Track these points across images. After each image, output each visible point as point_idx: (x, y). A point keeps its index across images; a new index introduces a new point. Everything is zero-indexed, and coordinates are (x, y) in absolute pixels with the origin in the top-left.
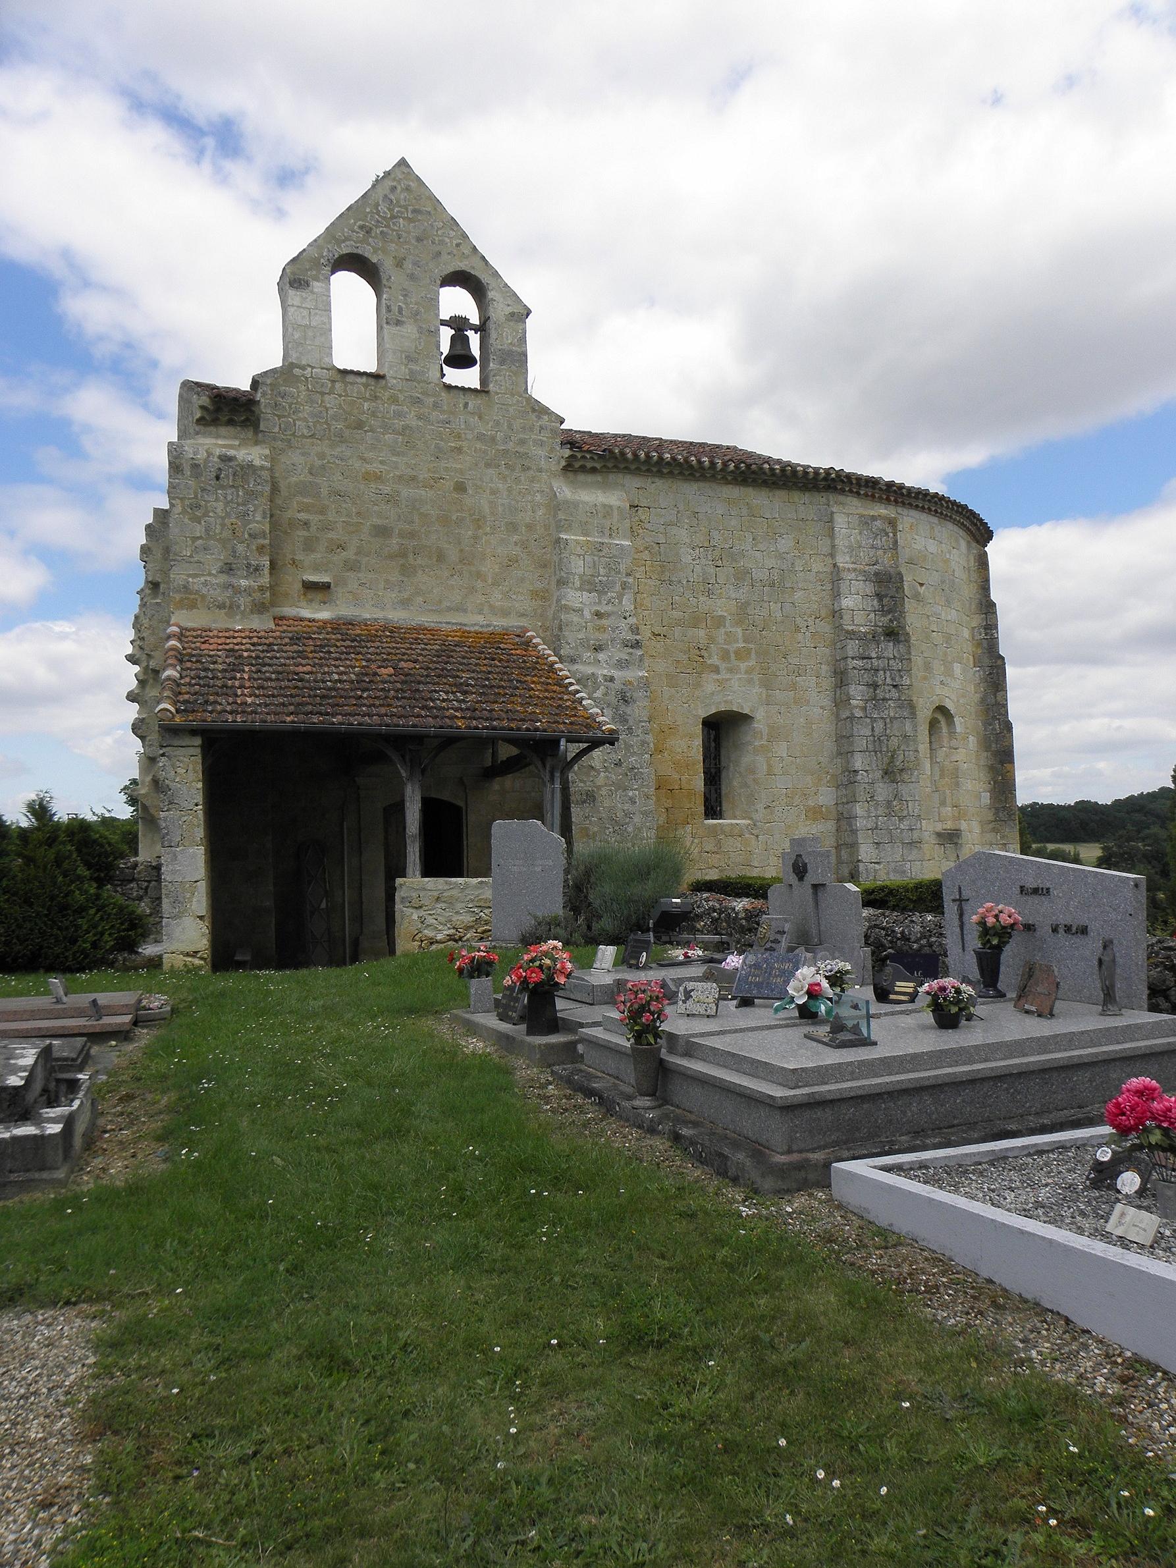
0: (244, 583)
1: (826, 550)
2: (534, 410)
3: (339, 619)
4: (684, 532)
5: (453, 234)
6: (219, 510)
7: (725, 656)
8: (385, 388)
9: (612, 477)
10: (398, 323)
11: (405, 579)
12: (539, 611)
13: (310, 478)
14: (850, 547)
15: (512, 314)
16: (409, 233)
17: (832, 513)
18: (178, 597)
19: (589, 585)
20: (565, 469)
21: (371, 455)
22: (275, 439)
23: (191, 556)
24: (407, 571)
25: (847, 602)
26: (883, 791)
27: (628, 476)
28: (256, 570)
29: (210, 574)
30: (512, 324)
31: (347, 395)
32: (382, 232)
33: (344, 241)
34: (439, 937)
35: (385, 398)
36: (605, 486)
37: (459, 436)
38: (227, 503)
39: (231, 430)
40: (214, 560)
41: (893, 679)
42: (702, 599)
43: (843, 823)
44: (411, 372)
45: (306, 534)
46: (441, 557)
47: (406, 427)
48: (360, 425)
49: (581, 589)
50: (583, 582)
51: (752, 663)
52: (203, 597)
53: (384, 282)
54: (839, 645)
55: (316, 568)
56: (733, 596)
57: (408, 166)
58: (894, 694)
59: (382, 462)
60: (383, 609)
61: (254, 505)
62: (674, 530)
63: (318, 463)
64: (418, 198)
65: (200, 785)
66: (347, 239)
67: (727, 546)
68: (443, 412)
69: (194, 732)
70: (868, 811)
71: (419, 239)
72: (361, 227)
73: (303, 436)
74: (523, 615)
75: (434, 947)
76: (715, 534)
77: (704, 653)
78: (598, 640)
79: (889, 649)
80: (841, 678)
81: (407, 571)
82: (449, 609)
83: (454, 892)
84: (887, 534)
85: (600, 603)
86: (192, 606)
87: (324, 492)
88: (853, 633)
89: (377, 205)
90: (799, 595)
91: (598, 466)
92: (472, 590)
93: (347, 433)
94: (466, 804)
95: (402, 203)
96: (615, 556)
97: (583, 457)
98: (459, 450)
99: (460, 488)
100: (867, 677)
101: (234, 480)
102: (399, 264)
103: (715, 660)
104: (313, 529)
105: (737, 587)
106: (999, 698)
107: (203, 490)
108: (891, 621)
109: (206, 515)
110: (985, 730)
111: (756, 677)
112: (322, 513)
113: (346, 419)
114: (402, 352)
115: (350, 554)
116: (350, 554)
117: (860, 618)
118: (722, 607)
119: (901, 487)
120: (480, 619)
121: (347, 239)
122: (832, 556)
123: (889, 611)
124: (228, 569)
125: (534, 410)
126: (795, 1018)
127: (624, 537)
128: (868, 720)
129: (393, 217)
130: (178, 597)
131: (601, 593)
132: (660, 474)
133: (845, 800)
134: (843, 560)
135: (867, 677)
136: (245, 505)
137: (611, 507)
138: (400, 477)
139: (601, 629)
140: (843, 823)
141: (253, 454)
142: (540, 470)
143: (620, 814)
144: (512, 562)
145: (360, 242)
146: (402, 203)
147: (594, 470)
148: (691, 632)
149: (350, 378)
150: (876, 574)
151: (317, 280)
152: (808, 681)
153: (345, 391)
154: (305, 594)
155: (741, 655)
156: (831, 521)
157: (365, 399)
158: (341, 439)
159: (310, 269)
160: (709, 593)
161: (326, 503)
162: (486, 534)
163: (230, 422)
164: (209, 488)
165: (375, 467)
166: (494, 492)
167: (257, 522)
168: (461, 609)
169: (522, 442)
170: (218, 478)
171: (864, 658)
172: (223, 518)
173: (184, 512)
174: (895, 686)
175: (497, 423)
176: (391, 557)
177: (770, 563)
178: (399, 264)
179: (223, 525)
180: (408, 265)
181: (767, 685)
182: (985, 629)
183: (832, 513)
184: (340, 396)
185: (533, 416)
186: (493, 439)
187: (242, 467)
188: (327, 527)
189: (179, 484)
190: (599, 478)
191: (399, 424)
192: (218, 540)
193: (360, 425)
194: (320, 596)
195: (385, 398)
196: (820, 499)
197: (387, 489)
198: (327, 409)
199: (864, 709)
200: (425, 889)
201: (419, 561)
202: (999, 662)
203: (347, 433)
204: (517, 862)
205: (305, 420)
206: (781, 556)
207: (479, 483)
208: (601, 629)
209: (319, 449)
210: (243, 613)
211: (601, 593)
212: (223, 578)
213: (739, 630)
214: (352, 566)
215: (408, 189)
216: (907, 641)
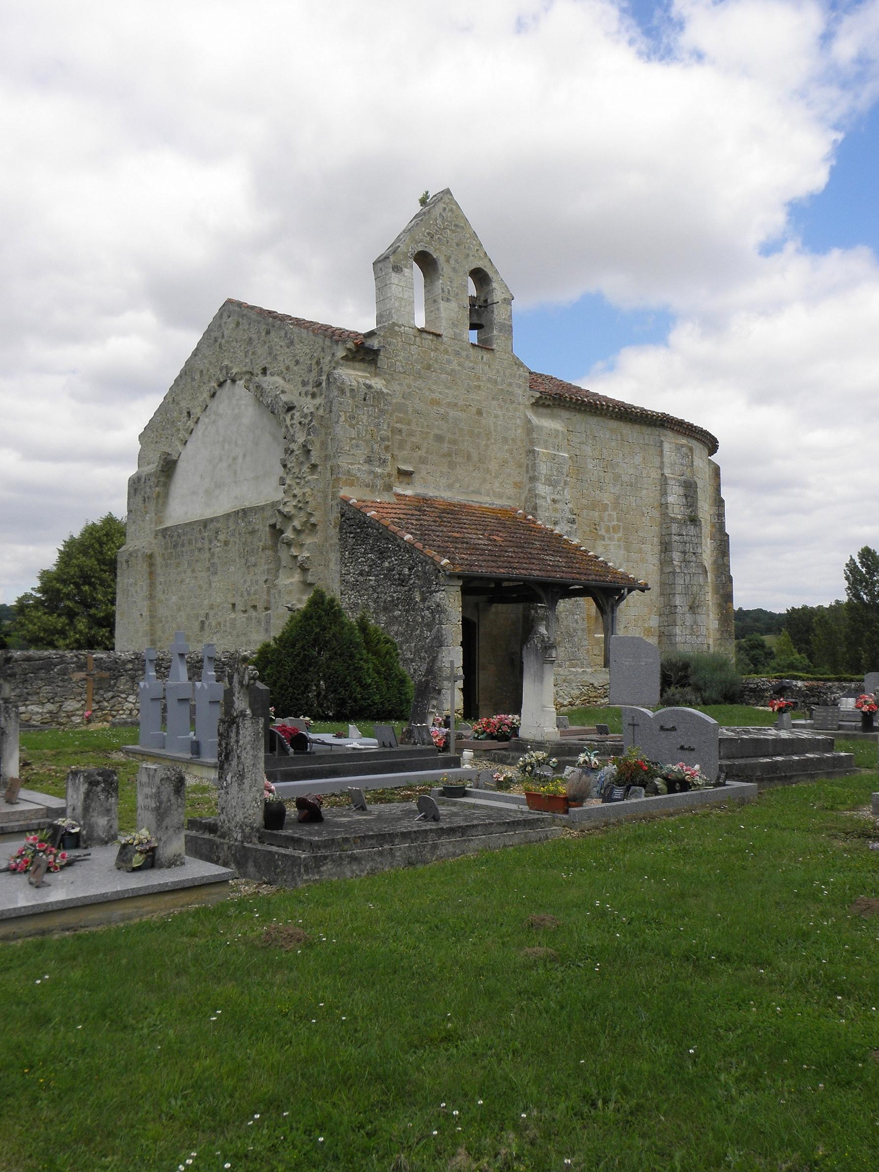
0: (379, 470)
1: (658, 464)
2: (516, 364)
3: (418, 495)
4: (589, 449)
5: (475, 242)
6: (364, 421)
7: (608, 531)
8: (442, 343)
9: (555, 410)
10: (448, 300)
11: (451, 471)
12: (518, 496)
13: (403, 401)
14: (671, 464)
15: (505, 299)
16: (452, 239)
17: (662, 441)
18: (344, 477)
19: (550, 482)
20: (533, 404)
21: (434, 387)
22: (385, 373)
23: (349, 451)
24: (452, 466)
25: (671, 499)
26: (689, 618)
27: (563, 411)
28: (384, 462)
29: (359, 463)
30: (505, 305)
31: (422, 347)
32: (439, 238)
33: (419, 242)
34: (565, 703)
35: (442, 350)
36: (553, 417)
37: (479, 379)
38: (369, 416)
39: (362, 365)
40: (361, 453)
41: (693, 549)
42: (598, 492)
43: (665, 639)
44: (455, 334)
45: (400, 437)
46: (469, 458)
47: (453, 370)
48: (429, 367)
49: (544, 484)
50: (546, 479)
51: (620, 535)
52: (358, 478)
53: (440, 272)
54: (664, 526)
55: (405, 462)
56: (612, 491)
57: (451, 195)
58: (694, 559)
59: (440, 393)
60: (439, 490)
61: (383, 419)
62: (584, 447)
63: (407, 391)
64: (457, 217)
65: (460, 609)
66: (421, 241)
67: (610, 459)
68: (471, 361)
69: (459, 577)
70: (682, 632)
71: (458, 245)
72: (429, 234)
73: (400, 372)
74: (509, 498)
75: (562, 708)
76: (604, 451)
77: (597, 527)
78: (556, 518)
79: (692, 530)
80: (666, 547)
81: (452, 466)
82: (473, 492)
83: (572, 677)
84: (688, 457)
85: (553, 493)
86: (352, 485)
87: (410, 410)
88: (674, 519)
89: (436, 219)
90: (644, 492)
91: (551, 403)
92: (485, 480)
93: (423, 372)
94: (479, 621)
95: (449, 219)
96: (561, 464)
97: (546, 398)
98: (479, 387)
99: (479, 413)
100: (681, 548)
101: (373, 401)
102: (448, 261)
103: (602, 532)
104: (404, 434)
105: (615, 485)
106: (725, 561)
107: (357, 407)
108: (691, 512)
109: (357, 423)
110: (717, 581)
111: (622, 544)
112: (409, 424)
113: (422, 362)
114: (450, 320)
115: (422, 453)
116: (422, 453)
117: (676, 510)
118: (607, 498)
119: (692, 425)
120: (487, 499)
121: (421, 241)
122: (662, 468)
123: (691, 506)
124: (369, 460)
125: (516, 364)
126: (856, 728)
127: (565, 451)
128: (683, 575)
129: (444, 228)
130: (344, 477)
131: (555, 487)
132: (579, 411)
133: (666, 624)
134: (667, 472)
135: (681, 548)
136: (378, 418)
137: (558, 431)
138: (449, 403)
139: (556, 510)
140: (665, 639)
141: (378, 383)
142: (519, 404)
143: (572, 630)
144: (504, 463)
145: (428, 243)
146: (449, 219)
147: (549, 406)
148: (592, 513)
149: (425, 335)
150: (685, 482)
151: (406, 267)
152: (647, 547)
153: (422, 343)
154: (398, 478)
155: (616, 529)
156: (661, 446)
157: (432, 350)
158: (419, 376)
159: (403, 260)
160: (601, 489)
161: (410, 417)
162: (492, 444)
163: (363, 360)
164: (360, 406)
165: (437, 396)
166: (496, 417)
167: (385, 430)
168: (478, 492)
169: (510, 384)
170: (365, 400)
171: (679, 535)
172: (367, 426)
173: (346, 420)
174: (694, 553)
175: (498, 371)
176: (444, 456)
177: (631, 471)
178: (448, 261)
179: (367, 431)
180: (452, 261)
181: (627, 549)
182: (718, 516)
183: (662, 441)
184: (419, 347)
185: (515, 368)
186: (496, 381)
187: (378, 393)
188: (411, 434)
189: (343, 402)
190: (549, 411)
191: (449, 368)
192: (363, 441)
193: (429, 367)
194: (406, 479)
195: (442, 350)
196: (656, 431)
197: (442, 411)
198: (412, 355)
199: (681, 567)
200: (559, 674)
201: (458, 460)
202: (726, 538)
203: (423, 372)
204: (628, 659)
205: (401, 361)
206: (636, 467)
207: (489, 410)
208: (556, 510)
209: (407, 381)
210: (379, 490)
211: (555, 487)
212: (366, 467)
213: (615, 513)
214: (423, 461)
215: (451, 210)
216: (700, 525)
